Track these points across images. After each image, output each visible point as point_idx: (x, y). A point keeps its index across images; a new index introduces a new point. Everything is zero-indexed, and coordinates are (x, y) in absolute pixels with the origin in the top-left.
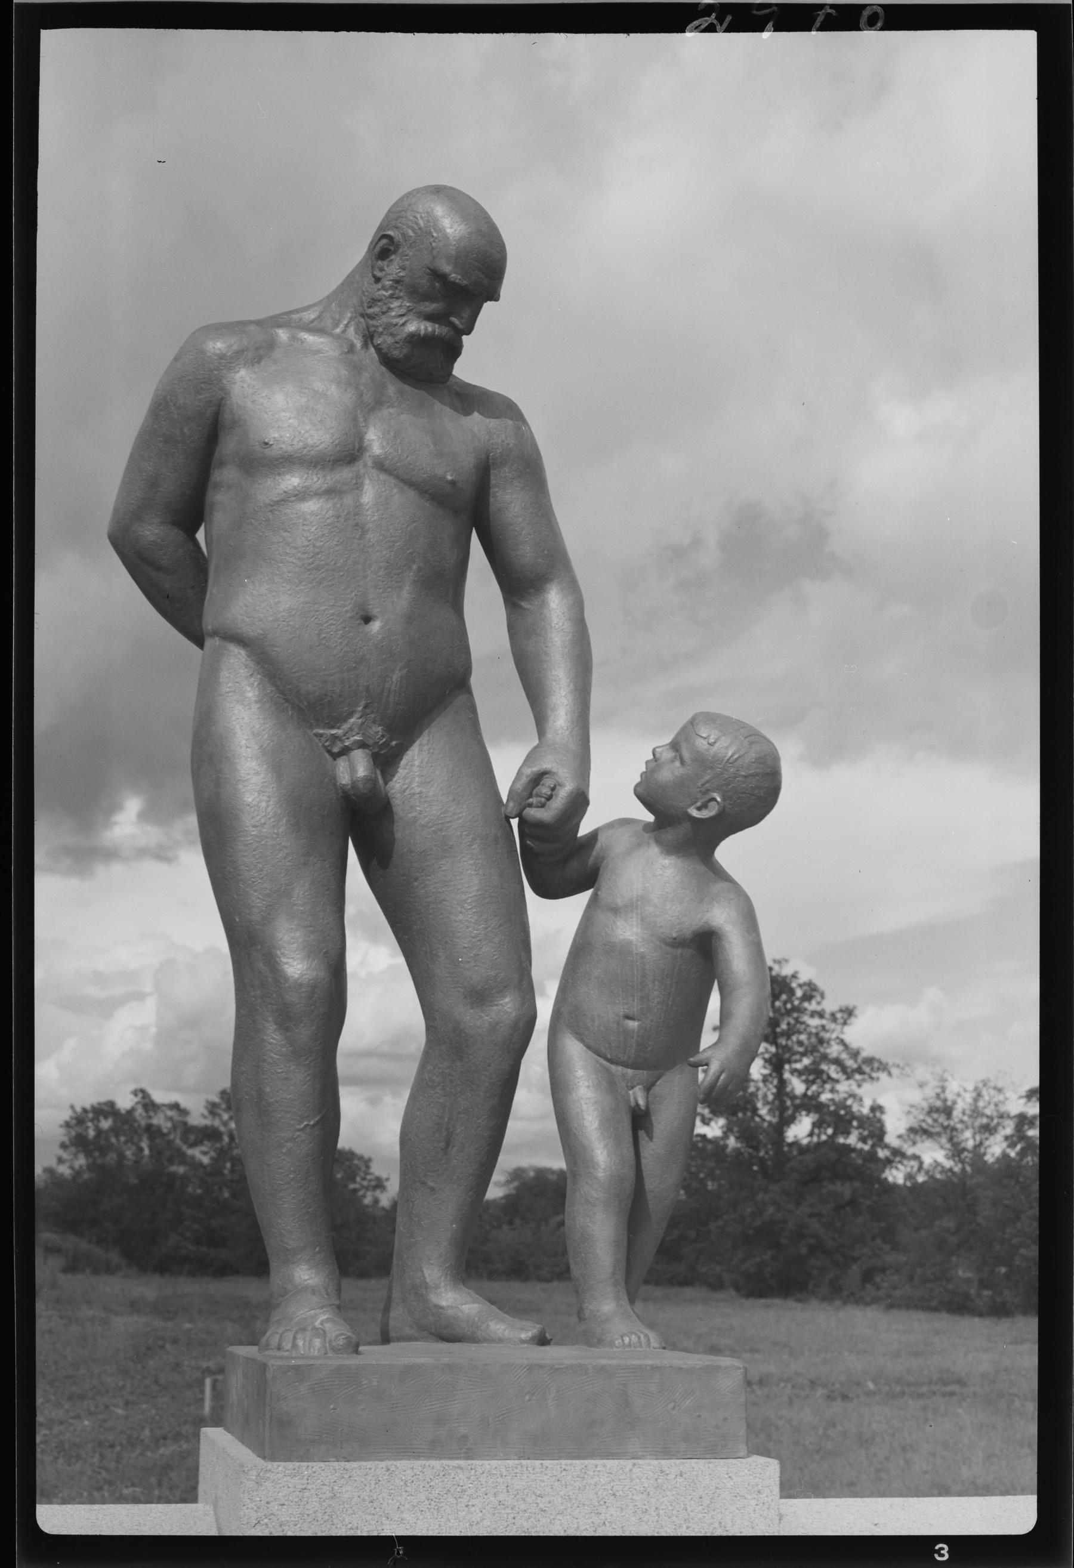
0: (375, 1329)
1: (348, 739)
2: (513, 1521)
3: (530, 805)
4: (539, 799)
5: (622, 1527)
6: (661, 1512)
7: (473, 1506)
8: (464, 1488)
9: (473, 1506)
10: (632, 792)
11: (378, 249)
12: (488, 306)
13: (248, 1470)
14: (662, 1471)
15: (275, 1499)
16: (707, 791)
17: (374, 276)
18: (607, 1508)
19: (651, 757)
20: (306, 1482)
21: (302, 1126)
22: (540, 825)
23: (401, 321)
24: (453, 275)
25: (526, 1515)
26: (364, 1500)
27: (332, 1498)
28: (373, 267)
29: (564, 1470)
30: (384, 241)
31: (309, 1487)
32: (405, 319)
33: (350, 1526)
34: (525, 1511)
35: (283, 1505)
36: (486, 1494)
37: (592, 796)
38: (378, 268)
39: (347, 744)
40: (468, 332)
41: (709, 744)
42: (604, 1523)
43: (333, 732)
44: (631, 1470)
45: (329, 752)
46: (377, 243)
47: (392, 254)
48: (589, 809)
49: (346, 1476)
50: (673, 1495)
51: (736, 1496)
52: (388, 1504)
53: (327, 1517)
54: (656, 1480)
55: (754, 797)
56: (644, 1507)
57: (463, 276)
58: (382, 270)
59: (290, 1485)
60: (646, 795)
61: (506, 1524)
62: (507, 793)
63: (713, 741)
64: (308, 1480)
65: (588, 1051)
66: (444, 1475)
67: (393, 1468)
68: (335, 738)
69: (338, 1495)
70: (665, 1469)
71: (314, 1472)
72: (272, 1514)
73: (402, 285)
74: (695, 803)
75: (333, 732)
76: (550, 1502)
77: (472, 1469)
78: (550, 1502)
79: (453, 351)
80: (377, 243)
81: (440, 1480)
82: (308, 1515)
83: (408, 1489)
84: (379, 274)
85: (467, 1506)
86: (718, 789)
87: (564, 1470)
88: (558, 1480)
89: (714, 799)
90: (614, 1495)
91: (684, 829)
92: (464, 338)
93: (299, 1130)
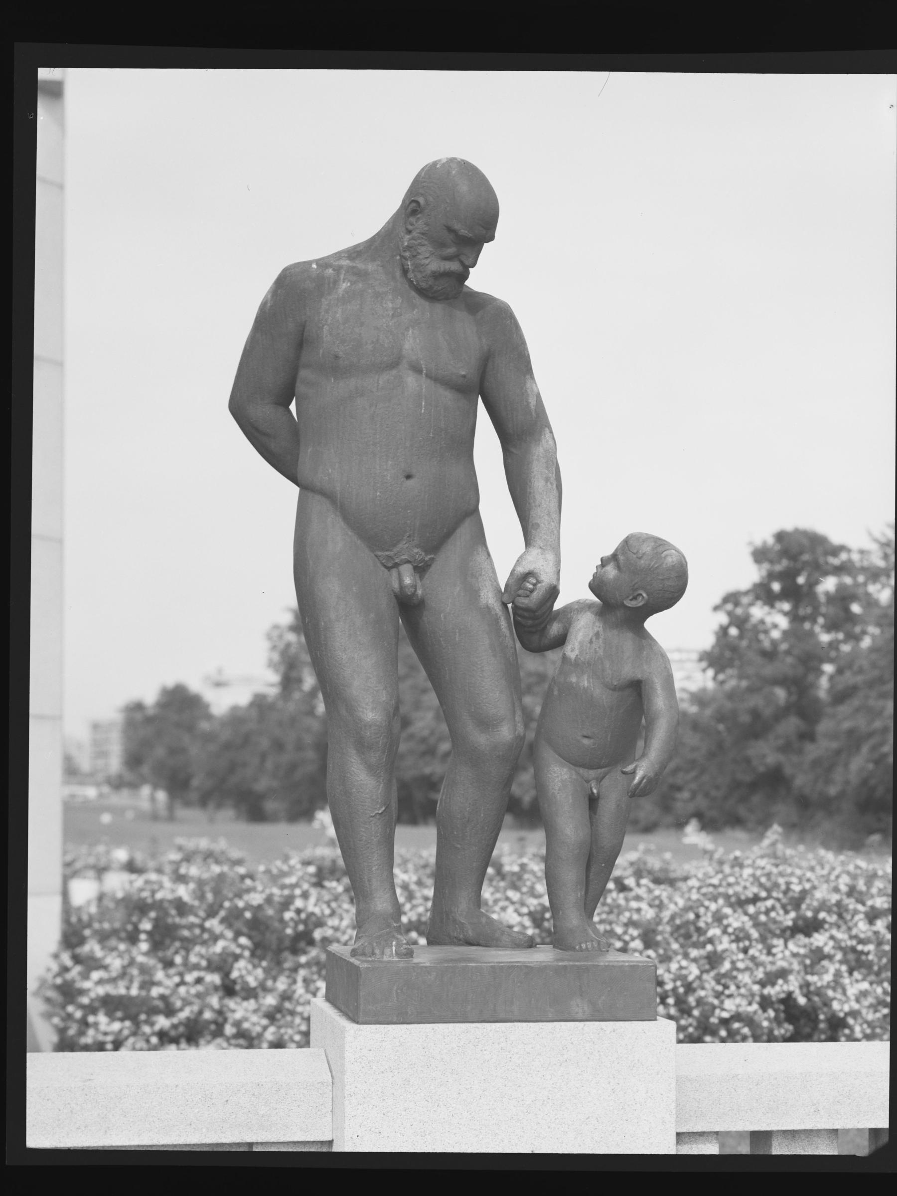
0: (621, 558)
1: (397, 558)
2: (510, 1059)
3: (519, 596)
4: (526, 592)
5: (577, 1063)
6: (602, 1054)
7: (485, 1050)
8: (480, 1039)
9: (485, 1050)
10: (592, 574)
11: (409, 210)
12: (487, 246)
13: (349, 1030)
14: (602, 1029)
15: (366, 1047)
16: (636, 590)
17: (407, 229)
18: (568, 1051)
19: (600, 563)
20: (383, 1036)
21: (374, 814)
22: (527, 609)
23: (427, 261)
24: (462, 231)
25: (518, 1056)
26: (419, 1047)
27: (399, 1046)
28: (405, 223)
29: (541, 1028)
30: (414, 205)
31: (385, 1039)
32: (429, 260)
33: (410, 1063)
34: (517, 1053)
35: (371, 1050)
36: (493, 1043)
37: (562, 588)
38: (410, 223)
39: (396, 561)
40: (473, 266)
41: (637, 558)
42: (566, 1060)
43: (387, 553)
44: (583, 1029)
45: (385, 566)
46: (408, 206)
47: (418, 214)
48: (559, 595)
49: (408, 1033)
50: (609, 1043)
51: (648, 1044)
52: (433, 1049)
53: (396, 1058)
54: (598, 1034)
55: (668, 593)
56: (591, 1051)
57: (468, 231)
58: (412, 224)
59: (374, 1038)
60: (596, 586)
61: (506, 1061)
62: (504, 587)
63: (641, 556)
64: (385, 1035)
65: (256, 1141)
66: (467, 1032)
67: (437, 1028)
68: (389, 558)
69: (403, 1044)
70: (604, 1027)
71: (389, 1031)
72: (363, 1056)
73: (426, 236)
74: (628, 597)
75: (387, 553)
76: (532, 1048)
77: (484, 1028)
78: (532, 1048)
79: (465, 276)
80: (408, 206)
81: (465, 1035)
82: (385, 1056)
83: (445, 1040)
84: (410, 227)
85: (482, 1050)
86: (643, 588)
87: (541, 1028)
88: (537, 1035)
89: (641, 595)
90: (572, 1043)
91: (620, 613)
92: (471, 270)
93: (372, 817)
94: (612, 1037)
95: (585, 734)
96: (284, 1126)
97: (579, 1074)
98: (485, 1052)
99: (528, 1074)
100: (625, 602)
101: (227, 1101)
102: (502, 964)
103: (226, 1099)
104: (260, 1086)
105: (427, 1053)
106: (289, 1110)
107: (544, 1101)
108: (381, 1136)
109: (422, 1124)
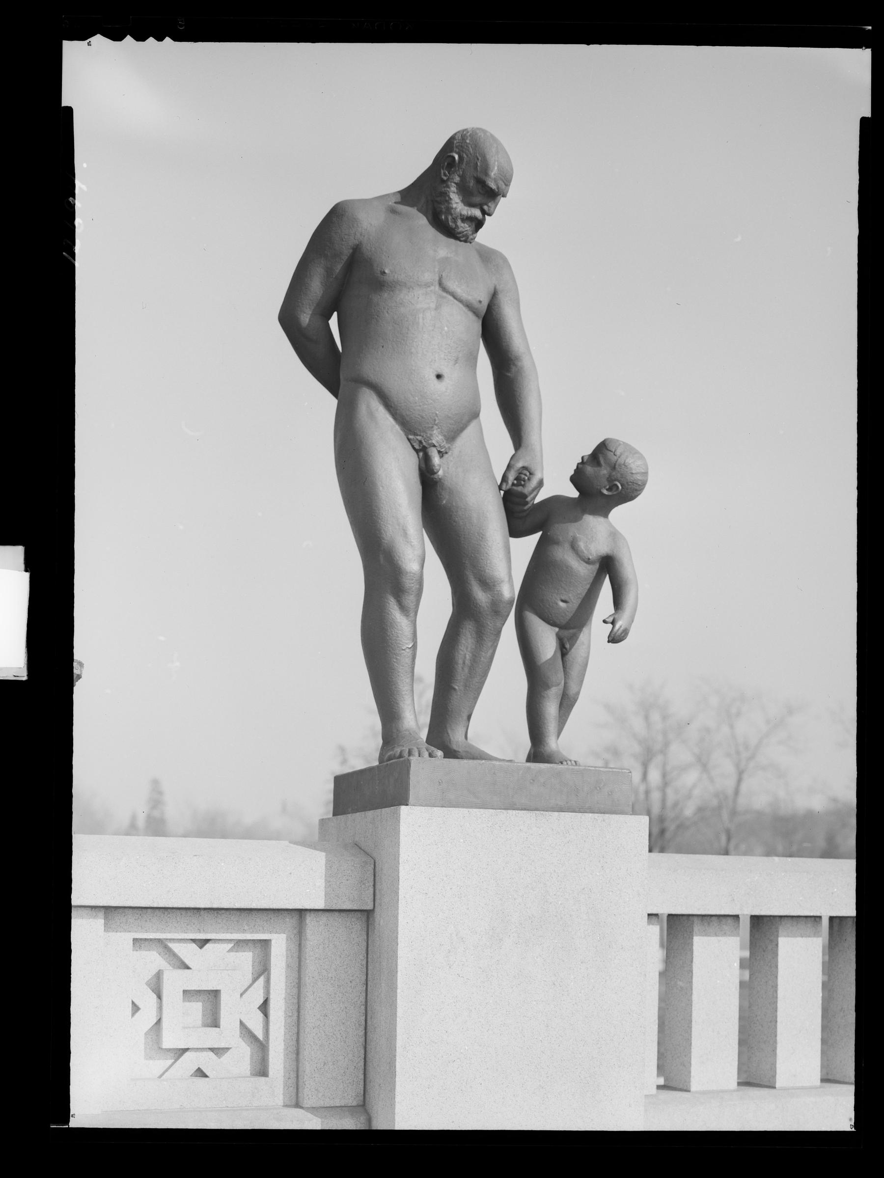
14: (595, 819)
94: (602, 825)
95: (563, 598)
96: (336, 896)
97: (578, 854)
98: (508, 833)
99: (540, 852)
100: (602, 490)
101: (291, 873)
102: (520, 764)
103: (290, 872)
104: (317, 862)
105: (464, 831)
106: (340, 883)
107: (551, 874)
108: (427, 896)
109: (459, 888)
